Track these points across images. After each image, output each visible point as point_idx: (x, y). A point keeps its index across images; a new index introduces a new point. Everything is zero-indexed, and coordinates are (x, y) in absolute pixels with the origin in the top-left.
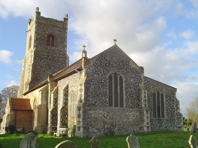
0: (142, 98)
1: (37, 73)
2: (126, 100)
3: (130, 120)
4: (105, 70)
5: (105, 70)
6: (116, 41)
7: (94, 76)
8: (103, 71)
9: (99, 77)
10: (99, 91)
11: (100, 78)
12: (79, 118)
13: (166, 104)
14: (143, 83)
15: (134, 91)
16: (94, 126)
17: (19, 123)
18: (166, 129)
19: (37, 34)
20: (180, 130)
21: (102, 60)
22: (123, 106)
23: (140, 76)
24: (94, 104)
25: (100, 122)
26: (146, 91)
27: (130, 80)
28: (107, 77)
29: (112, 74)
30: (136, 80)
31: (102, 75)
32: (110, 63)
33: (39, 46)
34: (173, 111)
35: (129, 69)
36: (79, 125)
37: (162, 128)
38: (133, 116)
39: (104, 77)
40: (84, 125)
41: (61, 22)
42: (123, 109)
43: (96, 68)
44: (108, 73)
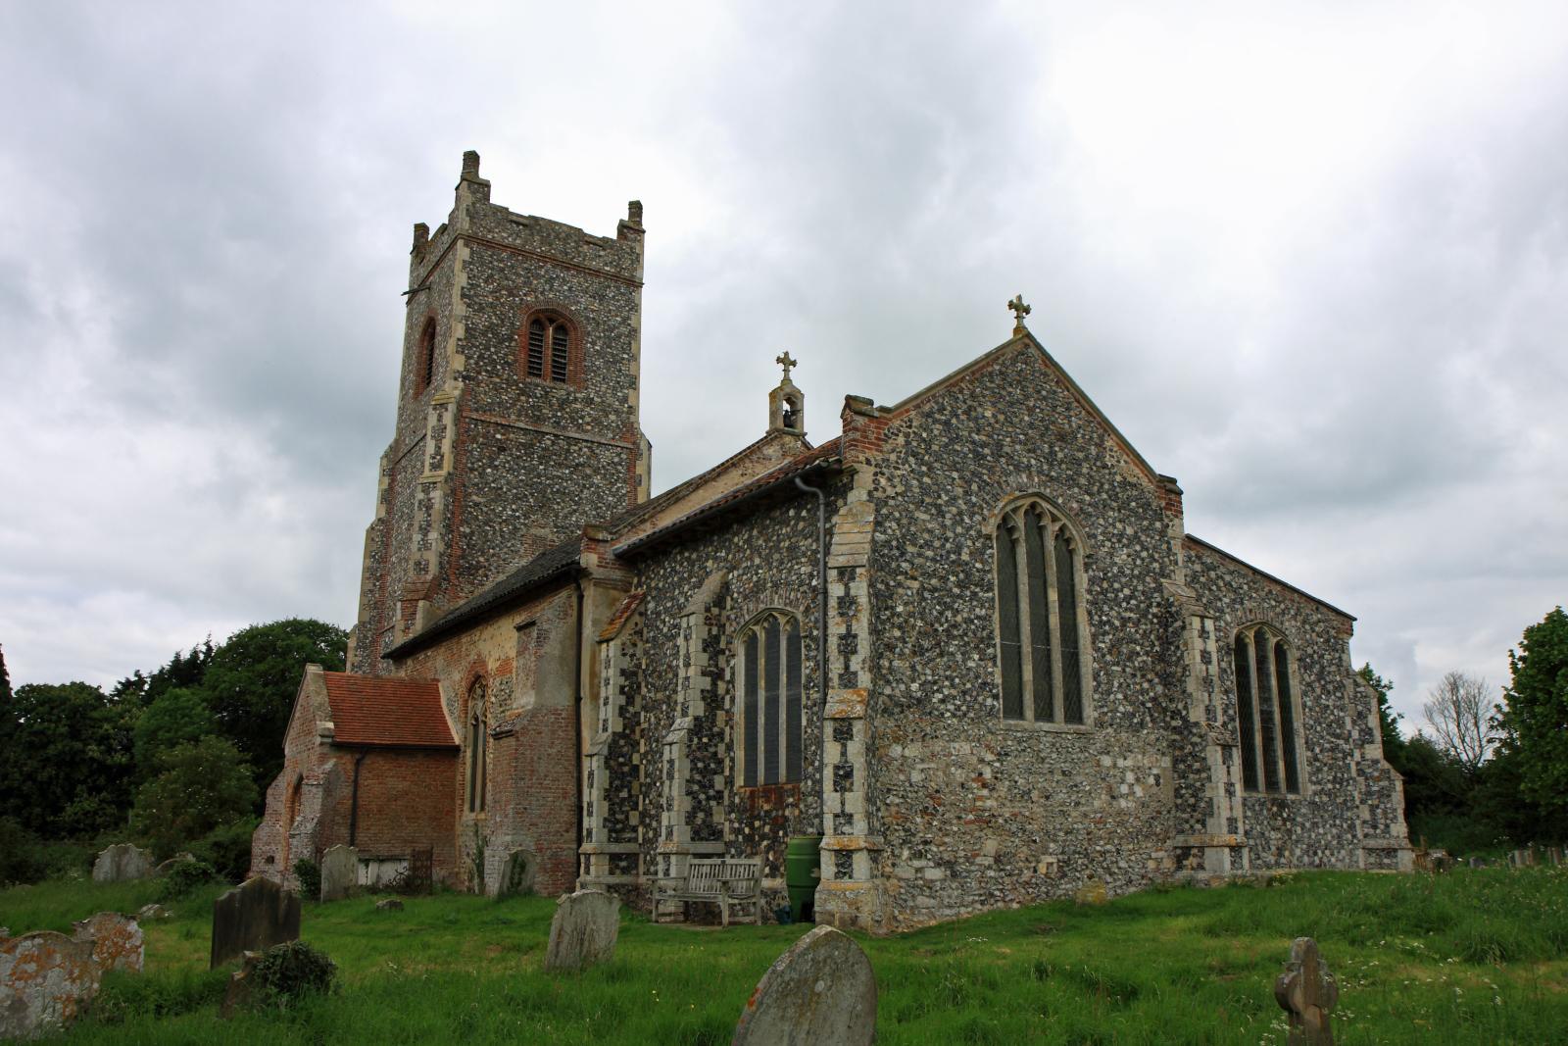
0: (1185, 668)
1: (472, 533)
2: (1095, 679)
3: (1123, 803)
4: (974, 487)
5: (974, 487)
6: (1027, 310)
7: (913, 520)
8: (966, 493)
9: (944, 526)
10: (949, 614)
11: (950, 534)
12: (843, 790)
13: (1304, 706)
14: (1180, 577)
15: (1137, 623)
16: (926, 843)
17: (374, 830)
18: (1312, 864)
19: (469, 306)
20: (1389, 866)
21: (954, 421)
22: (1081, 714)
23: (1163, 533)
24: (919, 701)
25: (959, 818)
26: (1209, 624)
27: (1112, 555)
28: (990, 528)
29: (1015, 510)
30: (1144, 554)
31: (960, 513)
32: (999, 445)
33: (483, 376)
34: (1344, 752)
35: (1106, 487)
36: (845, 840)
37: (1292, 854)
38: (1138, 780)
39: (971, 527)
40: (871, 839)
41: (604, 243)
42: (1081, 735)
43: (924, 468)
44: (991, 508)
